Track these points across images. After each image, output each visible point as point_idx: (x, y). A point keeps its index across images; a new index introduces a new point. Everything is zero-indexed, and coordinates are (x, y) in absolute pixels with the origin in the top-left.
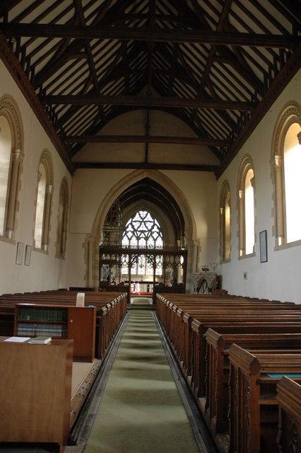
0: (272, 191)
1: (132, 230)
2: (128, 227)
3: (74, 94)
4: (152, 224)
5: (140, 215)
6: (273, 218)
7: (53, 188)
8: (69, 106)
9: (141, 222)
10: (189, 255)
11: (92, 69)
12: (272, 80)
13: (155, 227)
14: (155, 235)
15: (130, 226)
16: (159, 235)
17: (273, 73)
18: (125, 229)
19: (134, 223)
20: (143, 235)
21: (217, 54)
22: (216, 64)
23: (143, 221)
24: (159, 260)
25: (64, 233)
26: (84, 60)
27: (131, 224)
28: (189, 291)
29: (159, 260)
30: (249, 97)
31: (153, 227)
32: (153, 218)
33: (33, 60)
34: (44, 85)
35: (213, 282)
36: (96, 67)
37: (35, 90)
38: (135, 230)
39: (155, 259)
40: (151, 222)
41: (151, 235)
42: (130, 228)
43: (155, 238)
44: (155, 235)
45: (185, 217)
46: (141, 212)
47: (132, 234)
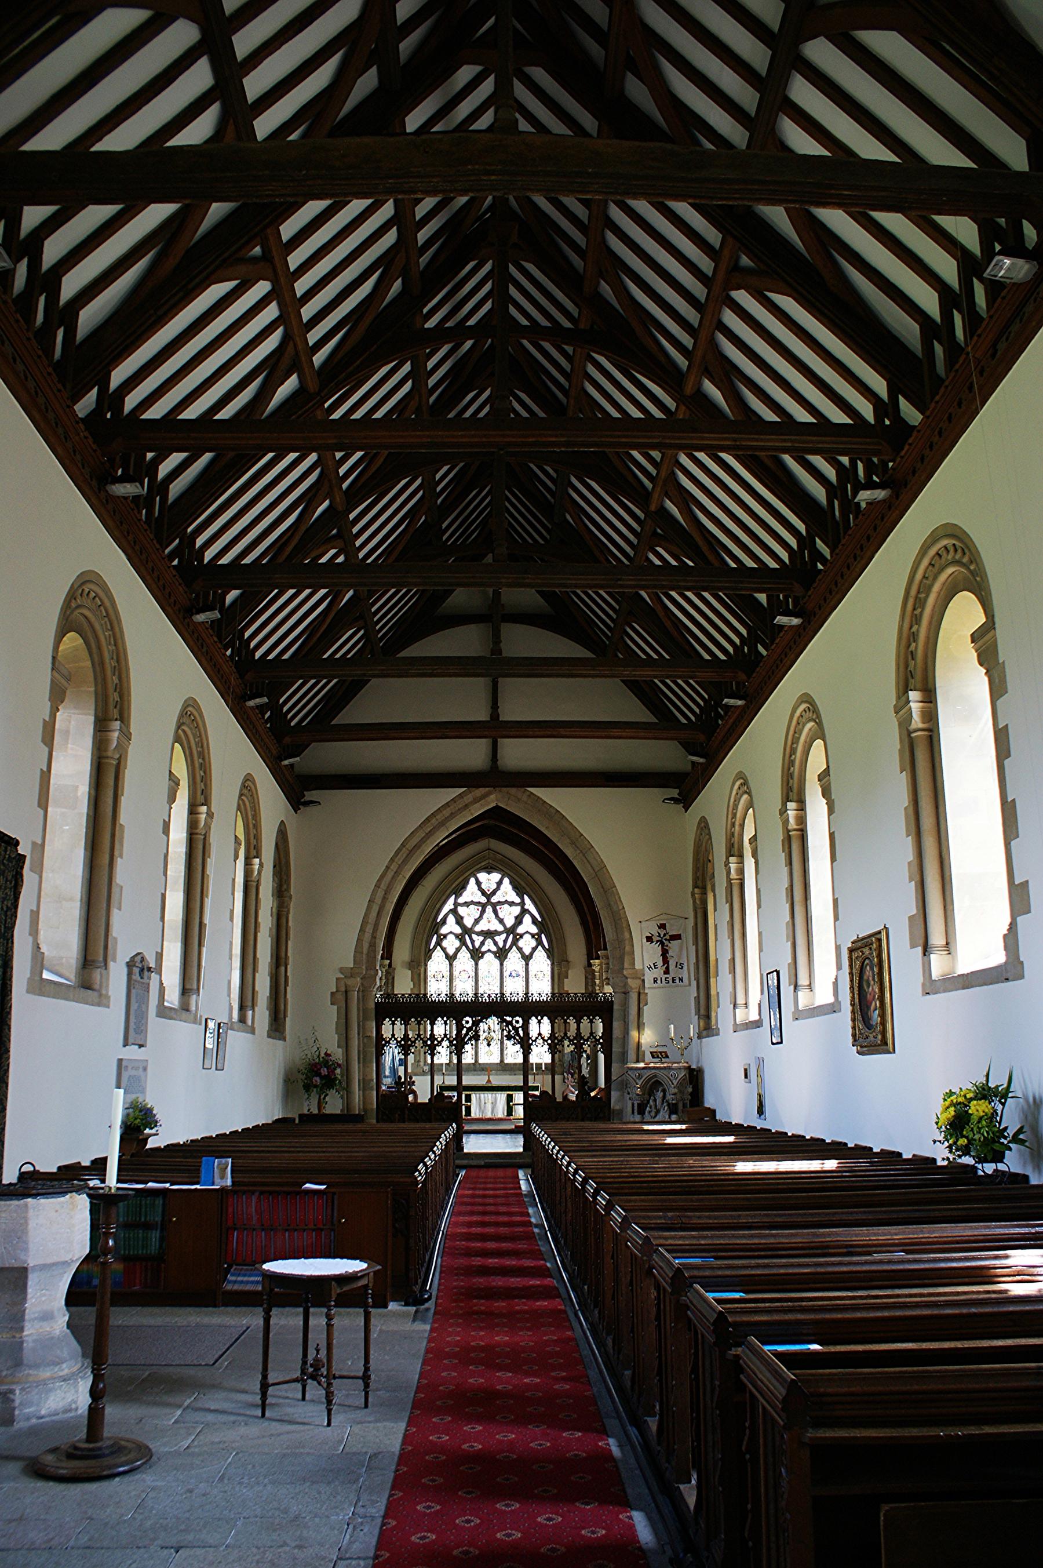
0: (786, 885)
1: (458, 930)
2: (444, 921)
3: (225, 414)
4: (517, 910)
5: (478, 883)
6: (789, 943)
7: (261, 865)
8: (208, 456)
9: (489, 897)
10: (616, 1014)
11: (288, 318)
12: (953, 350)
13: (527, 919)
14: (527, 944)
15: (451, 919)
16: (540, 943)
17: (979, 290)
18: (436, 927)
19: (462, 911)
20: (489, 945)
21: (745, 261)
22: (742, 297)
23: (489, 902)
24: (541, 1027)
25: (283, 969)
26: (262, 288)
27: (454, 911)
28: (620, 1112)
29: (541, 1027)
30: (867, 410)
31: (519, 920)
32: (520, 894)
33: (71, 284)
34: (118, 376)
35: (681, 1086)
36: (307, 312)
37: (77, 397)
38: (467, 931)
39: (526, 1027)
40: (512, 904)
41: (515, 943)
42: (451, 926)
43: (527, 951)
44: (527, 944)
45: (603, 914)
46: (482, 876)
47: (457, 943)
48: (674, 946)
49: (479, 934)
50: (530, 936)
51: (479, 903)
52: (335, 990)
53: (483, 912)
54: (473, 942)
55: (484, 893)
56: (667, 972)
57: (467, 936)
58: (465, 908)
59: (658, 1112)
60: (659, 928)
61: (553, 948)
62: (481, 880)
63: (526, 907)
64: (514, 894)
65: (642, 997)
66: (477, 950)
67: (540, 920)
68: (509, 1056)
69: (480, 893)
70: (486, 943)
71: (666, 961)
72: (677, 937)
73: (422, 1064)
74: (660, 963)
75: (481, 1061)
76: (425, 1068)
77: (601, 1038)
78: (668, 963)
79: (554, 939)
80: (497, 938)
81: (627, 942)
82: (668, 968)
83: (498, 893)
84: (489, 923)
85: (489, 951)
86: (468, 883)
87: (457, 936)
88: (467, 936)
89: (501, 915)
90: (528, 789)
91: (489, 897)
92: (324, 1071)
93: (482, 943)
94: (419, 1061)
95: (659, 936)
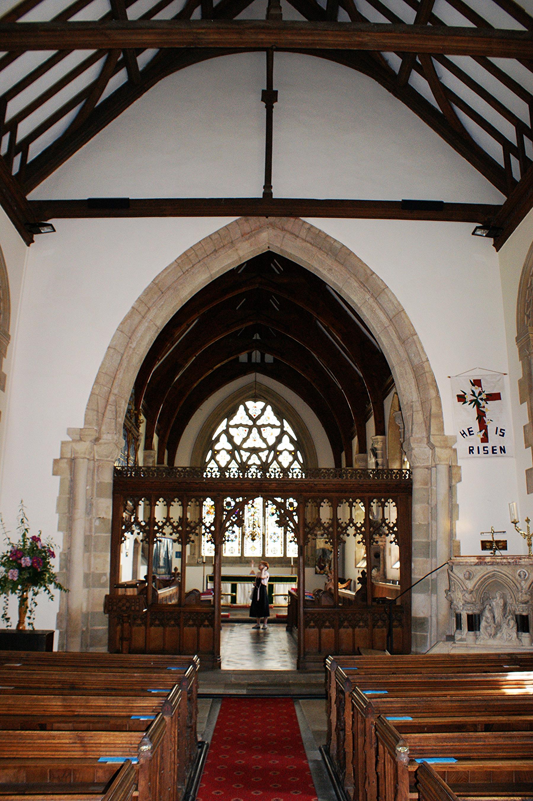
1: (229, 447)
2: (218, 440)
4: (277, 432)
5: (246, 410)
9: (254, 420)
13: (286, 439)
15: (224, 438)
16: (296, 458)
19: (232, 431)
20: (254, 460)
31: (279, 440)
32: (280, 419)
38: (237, 448)
40: (273, 426)
41: (275, 458)
42: (223, 444)
46: (250, 404)
48: (490, 407)
49: (246, 450)
50: (287, 453)
51: (247, 425)
52: (58, 457)
53: (250, 433)
54: (241, 456)
55: (250, 417)
56: (485, 439)
57: (236, 452)
58: (235, 429)
59: (498, 627)
60: (473, 385)
61: (307, 463)
62: (248, 407)
63: (285, 429)
64: (275, 418)
65: (454, 471)
66: (244, 463)
67: (296, 439)
68: (269, 551)
69: (247, 418)
70: (252, 457)
71: (483, 426)
72: (496, 397)
73: (196, 556)
74: (476, 427)
75: (245, 555)
76: (199, 560)
77: (395, 525)
78: (486, 428)
79: (308, 455)
80: (261, 454)
81: (433, 402)
82: (486, 435)
83: (262, 418)
84: (254, 441)
85: (254, 464)
86: (238, 409)
87: (228, 452)
88: (236, 452)
89: (264, 435)
90: (311, 221)
91: (254, 420)
92: (26, 561)
93: (249, 458)
94: (194, 554)
95: (474, 395)
